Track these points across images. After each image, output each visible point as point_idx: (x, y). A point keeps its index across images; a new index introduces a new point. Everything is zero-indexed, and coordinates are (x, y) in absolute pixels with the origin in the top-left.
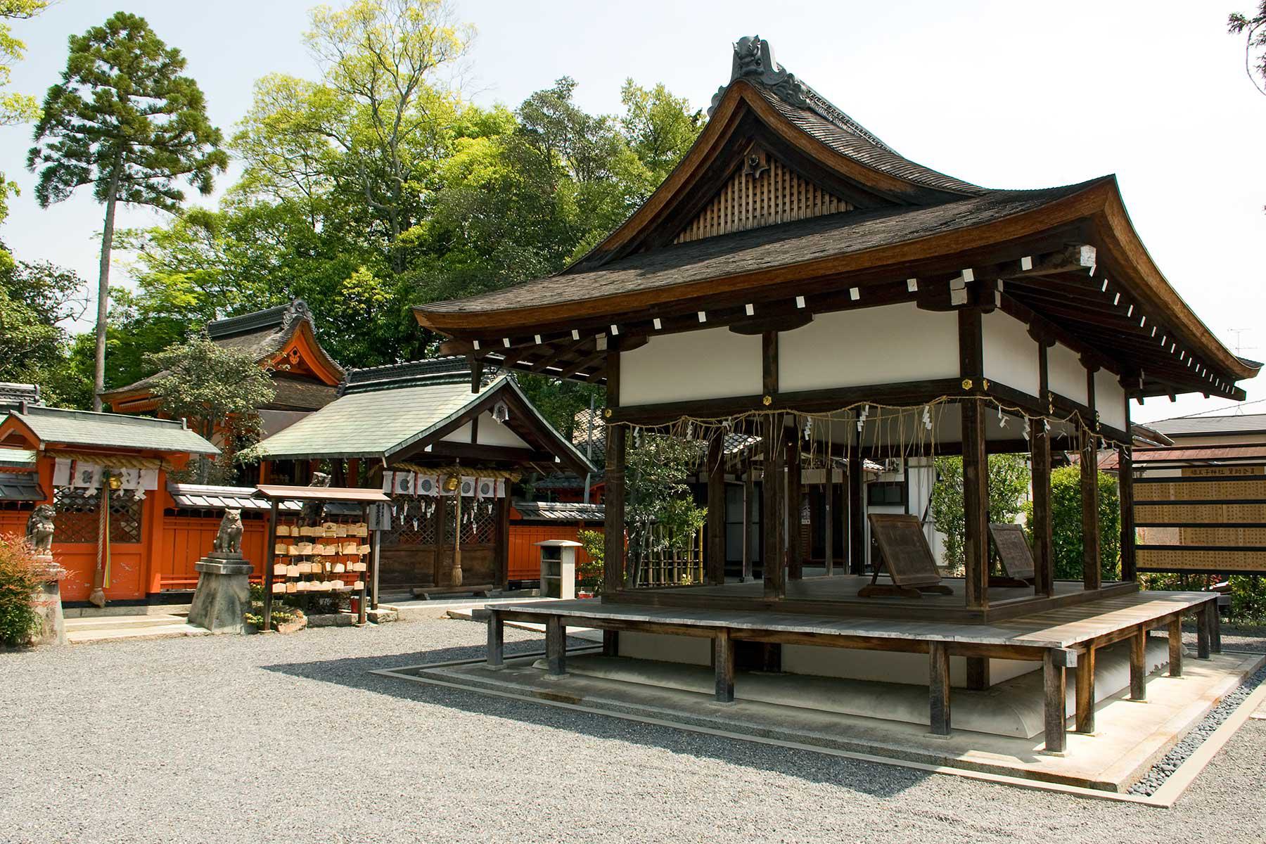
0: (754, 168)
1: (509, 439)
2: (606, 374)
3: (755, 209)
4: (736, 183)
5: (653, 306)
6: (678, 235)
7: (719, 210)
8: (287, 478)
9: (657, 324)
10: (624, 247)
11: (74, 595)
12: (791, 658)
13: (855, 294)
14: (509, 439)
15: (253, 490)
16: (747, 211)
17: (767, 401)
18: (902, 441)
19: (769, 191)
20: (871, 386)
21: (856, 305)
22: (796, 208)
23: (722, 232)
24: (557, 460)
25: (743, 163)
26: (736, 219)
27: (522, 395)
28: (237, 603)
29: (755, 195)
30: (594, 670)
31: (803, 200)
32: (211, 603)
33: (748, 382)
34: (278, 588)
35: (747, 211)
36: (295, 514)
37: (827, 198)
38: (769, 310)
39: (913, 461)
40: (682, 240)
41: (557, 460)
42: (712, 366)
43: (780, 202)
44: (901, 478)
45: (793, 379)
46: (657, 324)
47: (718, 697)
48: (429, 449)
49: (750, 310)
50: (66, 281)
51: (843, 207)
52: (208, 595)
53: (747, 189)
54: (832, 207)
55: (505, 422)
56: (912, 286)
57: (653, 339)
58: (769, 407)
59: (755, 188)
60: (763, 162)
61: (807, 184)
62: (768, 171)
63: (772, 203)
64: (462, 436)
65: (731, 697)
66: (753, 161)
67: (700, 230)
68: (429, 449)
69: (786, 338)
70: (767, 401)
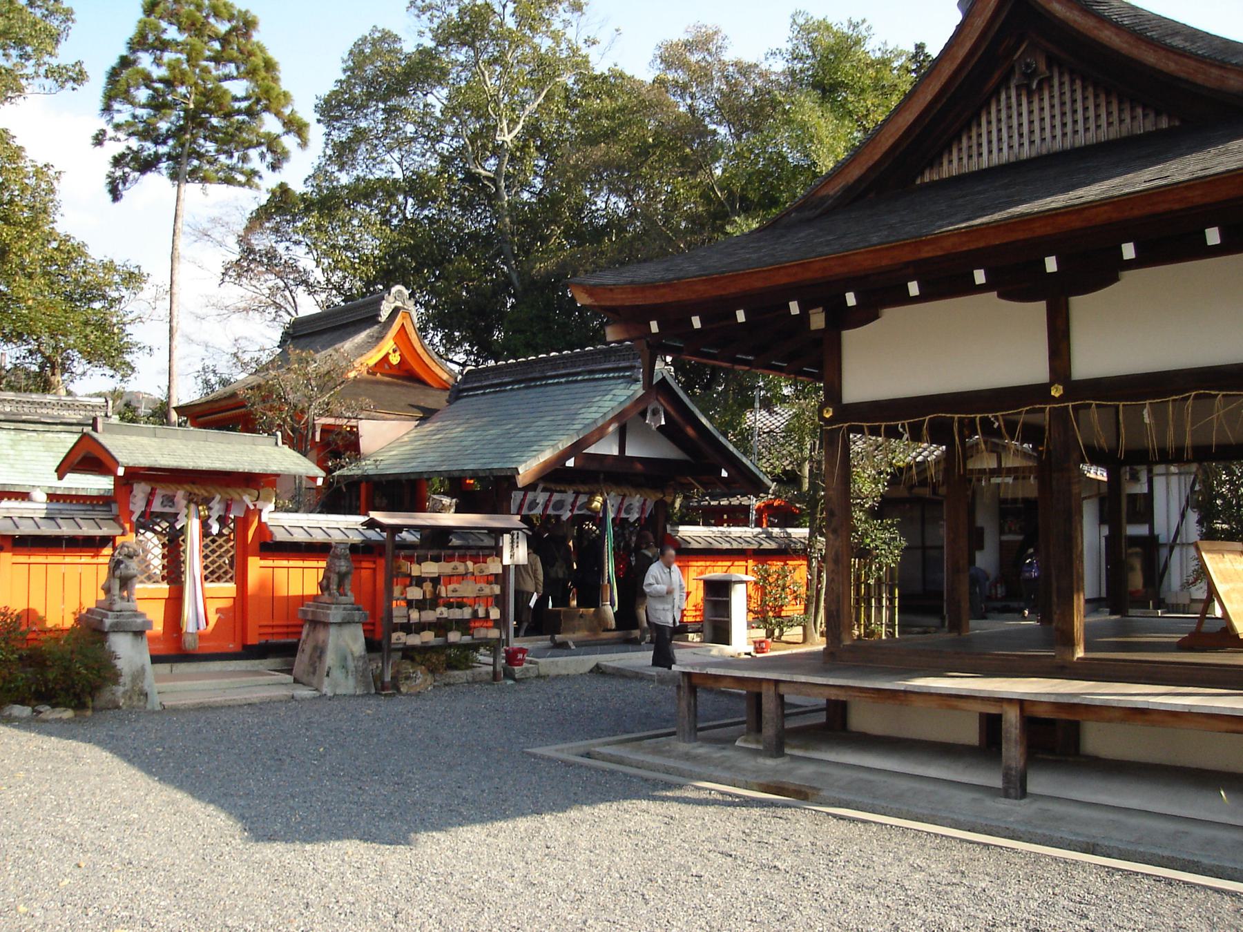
0: (1029, 76)
1: (664, 450)
2: (817, 361)
3: (1031, 132)
4: (1003, 96)
5: (908, 264)
6: (922, 174)
7: (980, 135)
8: (385, 501)
9: (1129, 251)
10: (849, 189)
11: (161, 649)
12: (1096, 740)
13: (1213, 236)
14: (664, 450)
15: (363, 519)
16: (1021, 135)
17: (1056, 392)
18: (1188, 442)
19: (1052, 106)
20: (1168, 372)
21: (915, 300)
22: (1093, 127)
23: (985, 165)
24: (724, 474)
25: (1013, 68)
26: (1005, 147)
27: (681, 394)
28: (350, 658)
29: (1031, 112)
30: (818, 749)
31: (1104, 116)
32: (320, 657)
33: (1024, 363)
34: (399, 638)
35: (1021, 135)
36: (411, 546)
37: (1139, 111)
38: (1059, 267)
39: (1158, 469)
40: (927, 180)
41: (724, 474)
42: (978, 347)
43: (1069, 120)
44: (1145, 490)
45: (1094, 358)
46: (1129, 251)
47: (1005, 793)
48: (570, 463)
49: (1051, 265)
50: (133, 278)
51: (1164, 124)
52: (315, 648)
53: (1019, 105)
54: (1141, 123)
55: (660, 428)
56: (980, 277)
57: (1128, 276)
58: (1061, 399)
59: (1030, 102)
60: (1042, 66)
61: (1108, 95)
62: (1050, 79)
63: (1058, 122)
64: (608, 448)
65: (1023, 794)
66: (1028, 66)
67: (951, 167)
68: (570, 463)
69: (1080, 305)
70: (1056, 392)
